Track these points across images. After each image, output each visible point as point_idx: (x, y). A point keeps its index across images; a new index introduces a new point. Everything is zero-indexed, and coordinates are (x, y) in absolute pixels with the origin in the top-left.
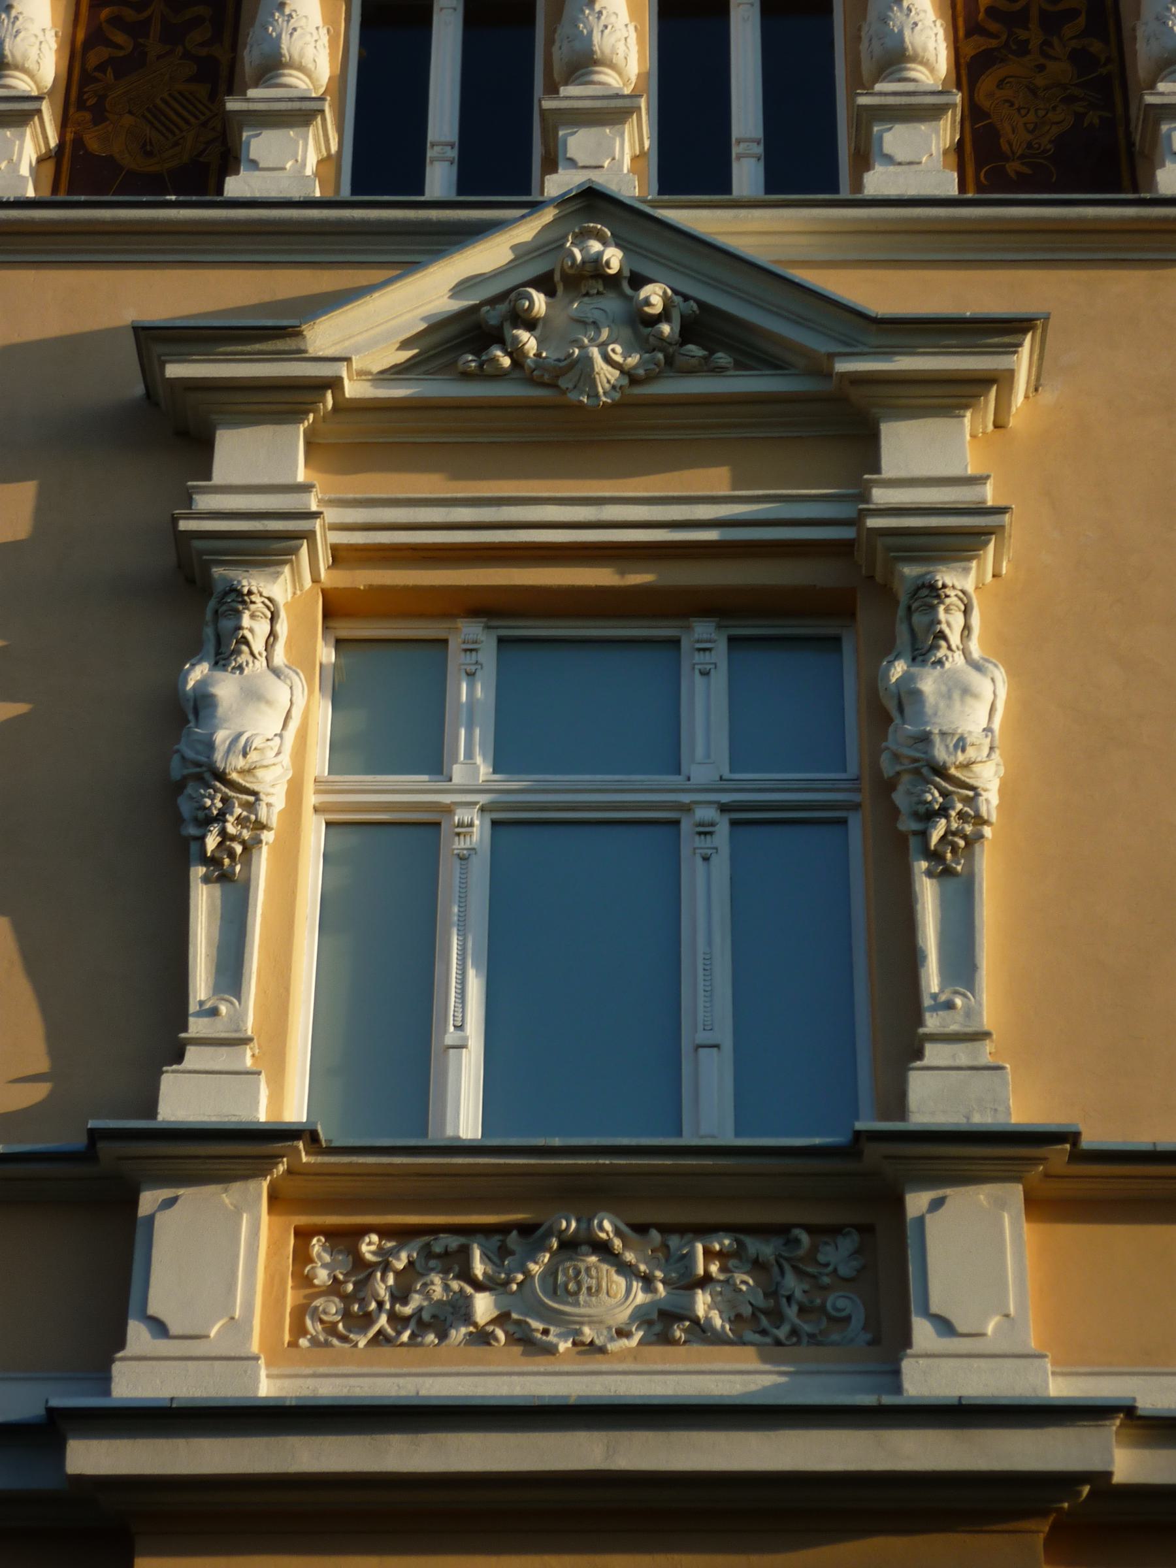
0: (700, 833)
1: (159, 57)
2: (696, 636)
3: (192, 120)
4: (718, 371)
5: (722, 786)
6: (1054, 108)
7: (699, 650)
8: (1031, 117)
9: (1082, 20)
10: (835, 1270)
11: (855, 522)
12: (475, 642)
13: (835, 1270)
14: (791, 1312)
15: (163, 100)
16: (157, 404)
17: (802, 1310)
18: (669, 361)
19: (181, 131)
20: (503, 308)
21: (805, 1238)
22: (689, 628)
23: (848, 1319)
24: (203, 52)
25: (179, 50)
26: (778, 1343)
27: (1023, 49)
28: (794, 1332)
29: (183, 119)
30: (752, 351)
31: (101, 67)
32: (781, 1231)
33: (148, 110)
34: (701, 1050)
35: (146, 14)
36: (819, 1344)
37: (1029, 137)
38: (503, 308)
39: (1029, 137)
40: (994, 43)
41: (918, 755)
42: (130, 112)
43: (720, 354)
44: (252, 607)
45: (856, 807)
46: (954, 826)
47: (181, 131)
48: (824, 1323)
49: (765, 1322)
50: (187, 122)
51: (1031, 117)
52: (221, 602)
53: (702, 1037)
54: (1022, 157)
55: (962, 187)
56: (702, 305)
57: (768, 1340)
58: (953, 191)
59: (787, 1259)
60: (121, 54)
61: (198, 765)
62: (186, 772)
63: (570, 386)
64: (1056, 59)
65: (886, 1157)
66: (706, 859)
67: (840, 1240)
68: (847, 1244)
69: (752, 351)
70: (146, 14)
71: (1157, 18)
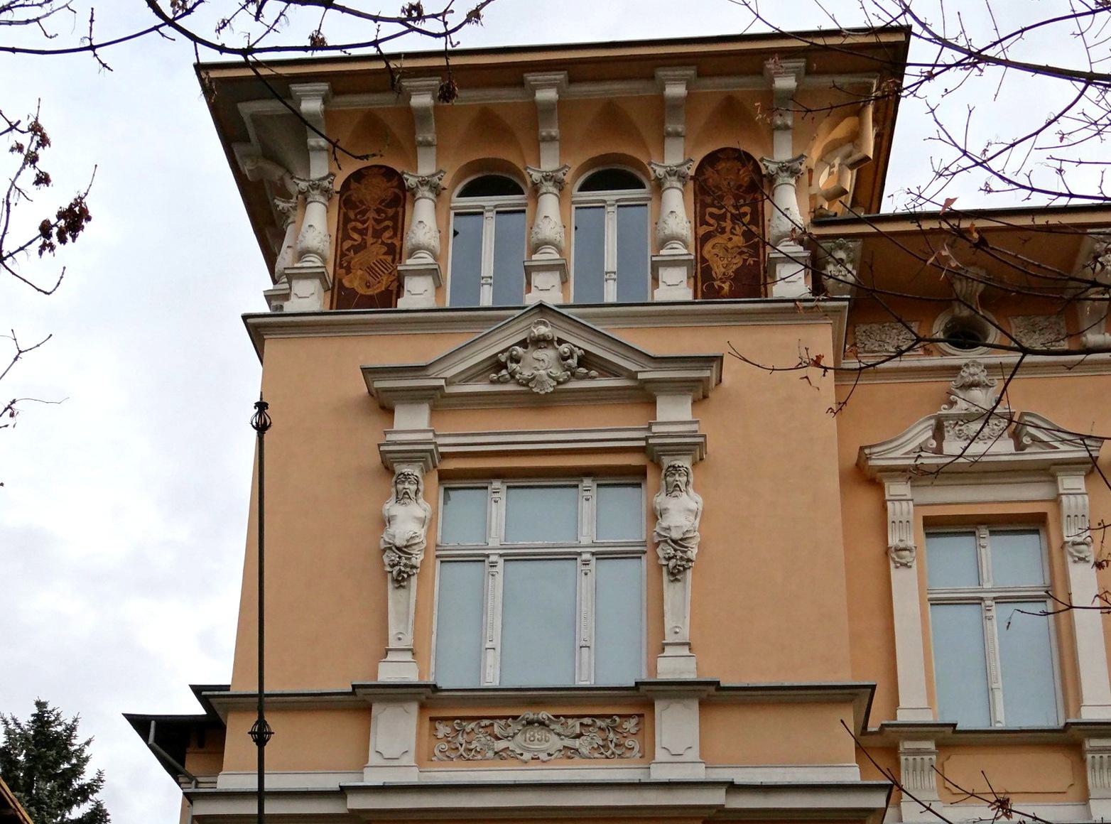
0: (584, 564)
1: (372, 244)
2: (584, 485)
3: (386, 272)
4: (593, 378)
5: (594, 545)
6: (735, 257)
7: (585, 490)
8: (725, 262)
9: (748, 217)
10: (629, 731)
11: (646, 439)
12: (498, 489)
13: (629, 731)
14: (612, 746)
15: (374, 263)
16: (373, 396)
17: (616, 745)
18: (573, 374)
19: (381, 276)
20: (507, 354)
21: (617, 719)
22: (582, 481)
23: (633, 748)
24: (390, 241)
25: (380, 240)
26: (607, 758)
27: (723, 231)
28: (613, 753)
29: (382, 271)
30: (608, 369)
31: (348, 250)
32: (610, 716)
33: (368, 268)
34: (583, 649)
35: (366, 225)
36: (622, 758)
37: (723, 270)
38: (507, 354)
39: (723, 270)
40: (711, 229)
41: (666, 535)
42: (361, 269)
43: (593, 372)
44: (409, 480)
45: (644, 552)
46: (679, 563)
47: (381, 276)
48: (624, 749)
49: (602, 750)
50: (384, 273)
51: (725, 262)
52: (397, 478)
53: (583, 643)
54: (721, 279)
55: (695, 296)
56: (585, 350)
57: (603, 756)
58: (690, 298)
59: (611, 727)
60: (356, 243)
61: (390, 544)
62: (386, 546)
63: (534, 386)
64: (737, 235)
65: (648, 691)
66: (586, 574)
67: (631, 720)
68: (634, 721)
69: (608, 369)
70: (366, 225)
71: (778, 218)
